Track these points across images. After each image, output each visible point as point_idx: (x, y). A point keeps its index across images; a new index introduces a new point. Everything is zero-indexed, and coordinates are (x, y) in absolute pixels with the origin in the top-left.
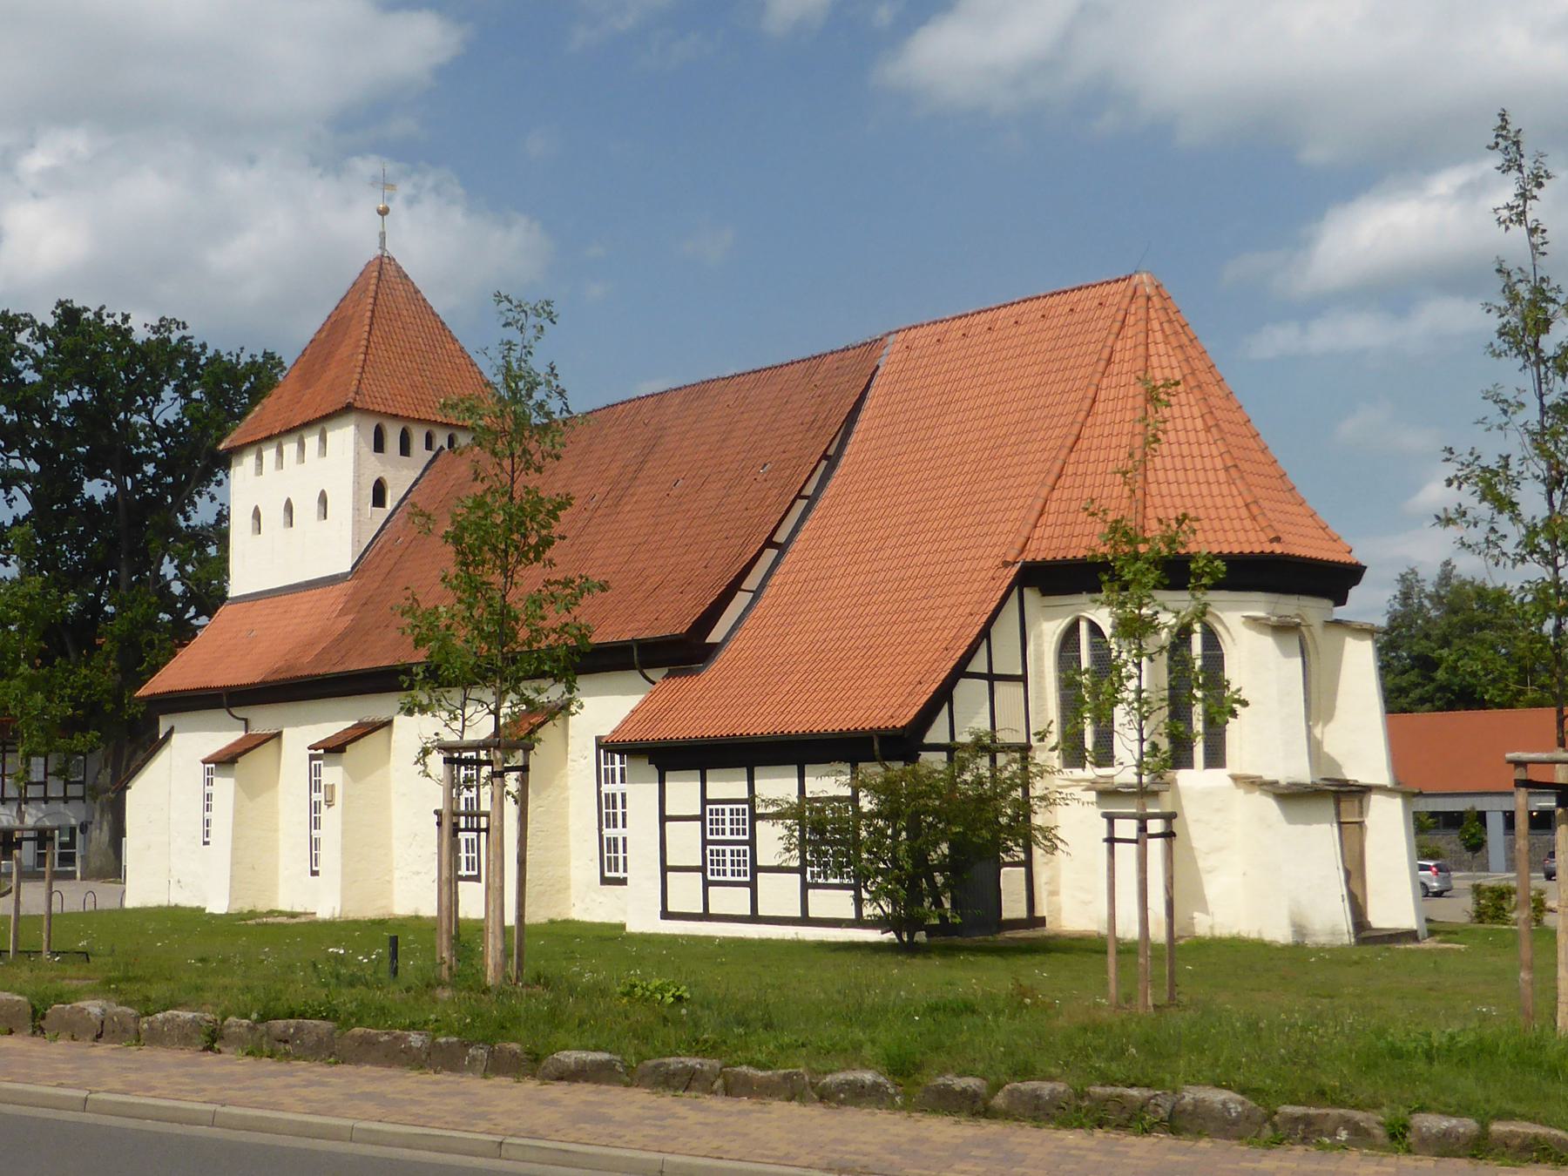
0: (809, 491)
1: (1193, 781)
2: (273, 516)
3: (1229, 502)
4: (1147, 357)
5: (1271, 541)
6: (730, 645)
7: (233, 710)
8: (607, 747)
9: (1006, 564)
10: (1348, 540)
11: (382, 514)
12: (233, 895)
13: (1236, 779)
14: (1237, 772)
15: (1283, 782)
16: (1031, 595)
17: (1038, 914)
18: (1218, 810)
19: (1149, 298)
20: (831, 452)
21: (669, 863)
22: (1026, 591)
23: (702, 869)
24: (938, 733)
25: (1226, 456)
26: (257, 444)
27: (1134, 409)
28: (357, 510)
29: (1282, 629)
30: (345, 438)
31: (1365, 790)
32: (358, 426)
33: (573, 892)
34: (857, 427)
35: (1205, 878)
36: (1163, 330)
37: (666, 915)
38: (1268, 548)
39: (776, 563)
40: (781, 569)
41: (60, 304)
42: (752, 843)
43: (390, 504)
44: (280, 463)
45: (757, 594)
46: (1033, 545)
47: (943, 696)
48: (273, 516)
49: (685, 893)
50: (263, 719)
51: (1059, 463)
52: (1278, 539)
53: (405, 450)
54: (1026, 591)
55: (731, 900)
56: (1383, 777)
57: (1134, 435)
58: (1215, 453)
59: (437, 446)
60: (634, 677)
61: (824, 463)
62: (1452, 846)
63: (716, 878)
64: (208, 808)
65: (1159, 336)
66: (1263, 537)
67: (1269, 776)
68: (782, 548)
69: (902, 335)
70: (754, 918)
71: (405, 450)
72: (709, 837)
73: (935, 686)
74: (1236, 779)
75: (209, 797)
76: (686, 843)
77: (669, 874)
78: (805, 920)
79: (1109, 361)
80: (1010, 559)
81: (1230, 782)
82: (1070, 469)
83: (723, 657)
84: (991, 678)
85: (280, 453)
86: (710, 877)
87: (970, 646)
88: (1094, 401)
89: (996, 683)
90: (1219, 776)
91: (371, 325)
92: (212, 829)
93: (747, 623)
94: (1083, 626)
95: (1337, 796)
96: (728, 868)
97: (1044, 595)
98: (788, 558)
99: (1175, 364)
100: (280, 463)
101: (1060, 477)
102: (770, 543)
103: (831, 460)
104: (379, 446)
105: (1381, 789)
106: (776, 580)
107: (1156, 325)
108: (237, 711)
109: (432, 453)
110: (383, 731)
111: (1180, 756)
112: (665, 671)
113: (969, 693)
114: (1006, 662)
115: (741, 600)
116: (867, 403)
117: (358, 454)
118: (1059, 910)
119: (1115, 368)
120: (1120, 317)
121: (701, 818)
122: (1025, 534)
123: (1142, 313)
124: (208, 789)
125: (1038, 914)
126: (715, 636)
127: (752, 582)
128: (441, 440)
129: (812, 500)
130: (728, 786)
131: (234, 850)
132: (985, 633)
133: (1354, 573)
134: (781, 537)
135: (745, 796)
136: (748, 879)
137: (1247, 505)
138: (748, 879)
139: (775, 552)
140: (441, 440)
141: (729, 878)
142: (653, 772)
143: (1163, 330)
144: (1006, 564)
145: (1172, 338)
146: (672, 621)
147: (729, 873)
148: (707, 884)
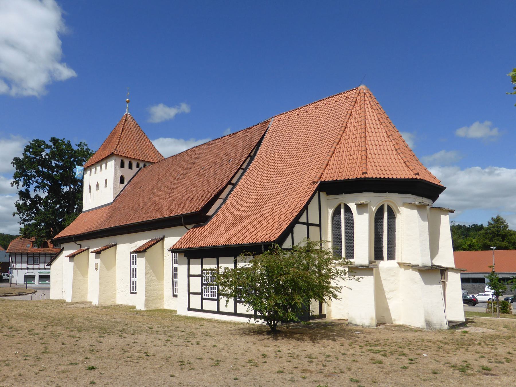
0: (244, 166)
1: (384, 264)
2: (94, 187)
3: (398, 161)
4: (365, 112)
5: (416, 174)
6: (215, 216)
8: (173, 251)
9: (314, 183)
11: (122, 186)
12: (73, 297)
13: (399, 264)
14: (400, 261)
16: (323, 195)
17: (323, 313)
18: (393, 276)
19: (365, 94)
20: (252, 154)
21: (191, 291)
22: (321, 193)
23: (201, 294)
24: (287, 244)
27: (361, 129)
28: (115, 184)
30: (112, 164)
33: (165, 299)
34: (261, 146)
35: (388, 301)
37: (189, 309)
38: (415, 177)
39: (232, 190)
40: (234, 192)
43: (126, 183)
44: (95, 173)
45: (225, 200)
46: (324, 176)
47: (289, 230)
48: (94, 187)
49: (196, 302)
50: (85, 244)
51: (333, 148)
52: (417, 174)
53: (130, 167)
54: (321, 193)
55: (210, 305)
56: (452, 265)
57: (361, 138)
58: (392, 144)
60: (182, 229)
61: (249, 158)
63: (205, 297)
65: (369, 106)
67: (414, 263)
68: (234, 185)
69: (276, 118)
70: (218, 312)
71: (130, 167)
72: (203, 282)
73: (286, 226)
74: (399, 264)
76: (196, 284)
77: (191, 295)
79: (351, 115)
80: (315, 180)
81: (397, 265)
82: (337, 150)
84: (308, 224)
85: (96, 170)
86: (204, 297)
87: (297, 215)
88: (346, 128)
95: (434, 273)
96: (210, 294)
98: (236, 188)
99: (375, 115)
100: (95, 173)
101: (333, 153)
102: (229, 183)
103: (251, 157)
104: (122, 166)
105: (452, 269)
106: (231, 195)
108: (78, 243)
109: (138, 169)
110: (114, 247)
111: (378, 255)
112: (193, 225)
113: (300, 231)
114: (314, 219)
115: (219, 202)
116: (266, 136)
118: (331, 312)
120: (354, 100)
121: (201, 276)
122: (321, 172)
123: (363, 98)
125: (323, 313)
126: (210, 213)
127: (223, 196)
128: (141, 165)
129: (245, 170)
130: (210, 265)
131: (73, 283)
132: (306, 207)
133: (440, 189)
134: (234, 181)
136: (216, 298)
137: (405, 162)
138: (216, 298)
139: (232, 186)
140: (141, 165)
141: (210, 297)
142: (186, 259)
144: (314, 183)
146: (194, 207)
147: (210, 295)
148: (203, 299)
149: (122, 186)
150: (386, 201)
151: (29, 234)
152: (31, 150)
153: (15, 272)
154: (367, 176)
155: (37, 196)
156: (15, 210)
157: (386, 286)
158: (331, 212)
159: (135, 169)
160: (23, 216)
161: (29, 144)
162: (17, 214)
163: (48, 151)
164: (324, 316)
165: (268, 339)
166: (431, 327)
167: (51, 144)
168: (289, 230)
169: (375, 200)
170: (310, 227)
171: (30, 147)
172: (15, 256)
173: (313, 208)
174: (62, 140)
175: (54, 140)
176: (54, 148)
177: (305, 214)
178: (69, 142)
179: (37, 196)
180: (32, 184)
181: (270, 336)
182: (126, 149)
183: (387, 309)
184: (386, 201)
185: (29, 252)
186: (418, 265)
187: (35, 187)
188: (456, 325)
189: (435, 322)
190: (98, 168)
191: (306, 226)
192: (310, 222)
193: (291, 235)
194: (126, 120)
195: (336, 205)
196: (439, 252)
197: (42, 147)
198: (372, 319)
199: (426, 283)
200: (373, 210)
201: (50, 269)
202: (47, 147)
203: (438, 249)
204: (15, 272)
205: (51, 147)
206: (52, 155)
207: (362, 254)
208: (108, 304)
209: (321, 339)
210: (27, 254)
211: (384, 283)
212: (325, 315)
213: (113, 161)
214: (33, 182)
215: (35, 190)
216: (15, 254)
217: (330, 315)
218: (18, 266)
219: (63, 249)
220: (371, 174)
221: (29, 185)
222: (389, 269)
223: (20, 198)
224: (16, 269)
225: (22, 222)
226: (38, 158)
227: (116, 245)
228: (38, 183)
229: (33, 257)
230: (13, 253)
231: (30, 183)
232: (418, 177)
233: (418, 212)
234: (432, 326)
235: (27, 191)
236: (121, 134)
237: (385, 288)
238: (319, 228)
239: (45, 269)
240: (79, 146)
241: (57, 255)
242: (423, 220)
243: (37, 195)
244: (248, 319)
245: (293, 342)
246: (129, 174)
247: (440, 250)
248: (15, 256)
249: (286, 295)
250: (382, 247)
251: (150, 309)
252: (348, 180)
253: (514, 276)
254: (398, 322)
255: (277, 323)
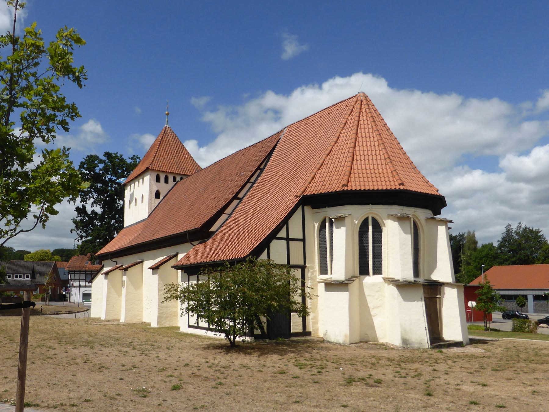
0: (252, 180)
5: (400, 185)
10: (436, 186)
13: (384, 279)
14: (386, 276)
15: (401, 280)
16: (307, 209)
17: (307, 330)
18: (377, 292)
19: (362, 101)
22: (306, 207)
25: (385, 154)
29: (401, 219)
30: (147, 178)
31: (443, 284)
32: (151, 175)
35: (373, 318)
36: (366, 112)
37: (189, 326)
38: (397, 187)
40: (239, 206)
43: (161, 198)
45: (230, 215)
47: (265, 245)
52: (402, 184)
53: (166, 181)
59: (177, 181)
60: (188, 245)
62: (124, 361)
65: (364, 114)
66: (396, 183)
68: (241, 199)
71: (166, 181)
74: (384, 279)
79: (345, 124)
80: (298, 195)
81: (382, 280)
83: (214, 237)
84: (288, 239)
88: (338, 138)
90: (378, 278)
91: (159, 146)
93: (226, 224)
94: (327, 220)
97: (313, 209)
103: (260, 169)
104: (158, 180)
107: (364, 110)
108: (114, 260)
111: (364, 271)
112: (199, 242)
115: (223, 217)
117: (150, 183)
118: (318, 330)
119: (347, 126)
125: (307, 330)
126: (213, 229)
127: (228, 211)
128: (178, 178)
129: (253, 183)
134: (240, 196)
137: (392, 172)
139: (238, 201)
143: (366, 112)
144: (297, 196)
145: (369, 114)
146: (195, 223)
149: (158, 201)
150: (371, 213)
151: (85, 250)
152: (85, 166)
153: (73, 289)
154: (346, 188)
155: (93, 212)
156: (73, 226)
157: (371, 302)
158: (316, 225)
159: (171, 182)
160: (81, 232)
161: (84, 161)
162: (74, 230)
163: (101, 166)
164: (309, 334)
165: (221, 352)
166: (408, 346)
167: (104, 158)
168: (265, 245)
169: (355, 214)
170: (291, 242)
171: (84, 163)
172: (74, 274)
173: (295, 223)
174: (115, 154)
175: (107, 154)
176: (108, 162)
177: (285, 228)
178: (121, 156)
179: (93, 212)
180: (89, 199)
181: (222, 351)
182: (162, 164)
183: (372, 327)
184: (371, 213)
185: (87, 269)
186: (399, 280)
187: (92, 203)
188: (444, 345)
189: (413, 340)
190: (137, 183)
191: (286, 241)
192: (290, 237)
193: (266, 251)
194: (164, 133)
195: (321, 219)
196: (438, 266)
197: (96, 162)
198: (346, 336)
199: (405, 300)
200: (356, 223)
201: (91, 286)
202: (101, 161)
203: (436, 262)
204: (73, 289)
205: (104, 161)
206: (106, 170)
207: (339, 270)
208: (134, 321)
209: (285, 354)
210: (86, 271)
211: (369, 299)
212: (310, 332)
213: (149, 176)
214: (90, 197)
215: (92, 206)
216: (74, 271)
217: (317, 333)
218: (77, 284)
219: (103, 265)
220: (353, 186)
221: (86, 201)
222: (373, 285)
223: (78, 215)
224: (74, 287)
225: (79, 238)
226: (92, 173)
227: (142, 262)
228: (94, 198)
229: (91, 274)
230: (71, 271)
231: (87, 199)
232: (402, 187)
233: (399, 224)
234: (409, 344)
235: (84, 207)
236: (158, 148)
237: (370, 305)
238: (302, 243)
239: (85, 287)
240: (132, 159)
241: (98, 272)
242: (406, 233)
243: (93, 210)
244: (204, 331)
245: (242, 355)
246: (164, 188)
247: (438, 264)
248: (74, 274)
249: (258, 310)
250: (368, 261)
251: (163, 326)
252: (328, 192)
253: (547, 292)
254: (381, 341)
255: (235, 338)
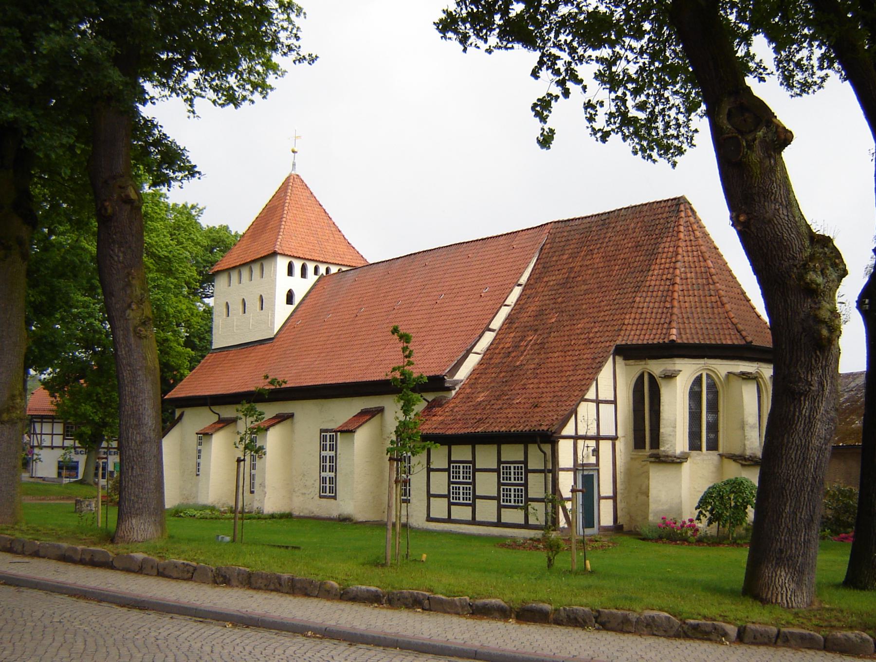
7: (212, 408)
11: (291, 308)
16: (619, 359)
26: (228, 270)
37: (429, 519)
41: (549, 148)
42: (526, 485)
49: (439, 508)
50: (228, 412)
53: (304, 274)
54: (617, 358)
64: (199, 457)
70: (473, 522)
71: (304, 274)
75: (199, 451)
76: (440, 482)
78: (499, 524)
89: (600, 405)
92: (201, 467)
110: (288, 421)
121: (497, 471)
124: (200, 448)
128: (322, 270)
135: (522, 459)
148: (450, 504)
